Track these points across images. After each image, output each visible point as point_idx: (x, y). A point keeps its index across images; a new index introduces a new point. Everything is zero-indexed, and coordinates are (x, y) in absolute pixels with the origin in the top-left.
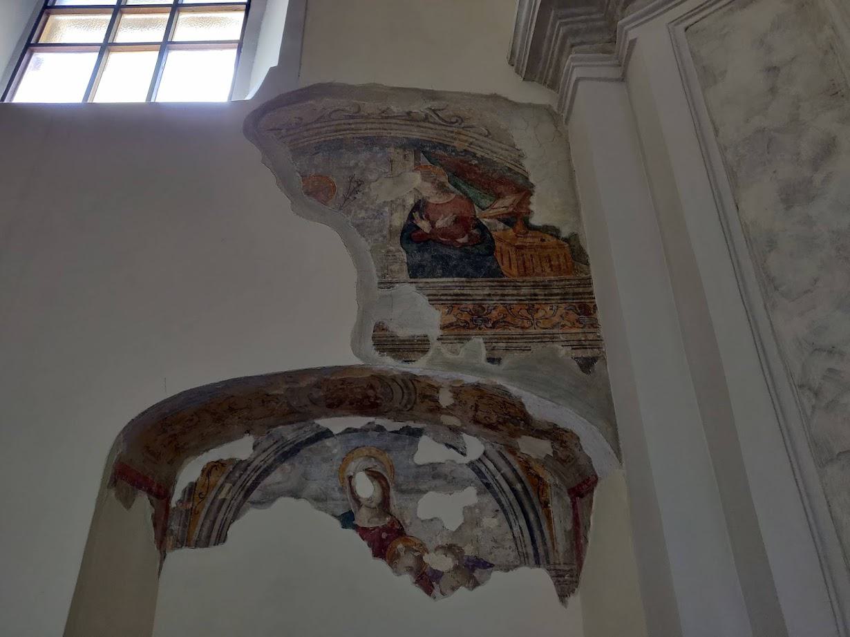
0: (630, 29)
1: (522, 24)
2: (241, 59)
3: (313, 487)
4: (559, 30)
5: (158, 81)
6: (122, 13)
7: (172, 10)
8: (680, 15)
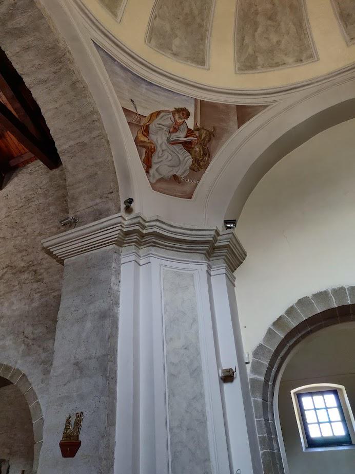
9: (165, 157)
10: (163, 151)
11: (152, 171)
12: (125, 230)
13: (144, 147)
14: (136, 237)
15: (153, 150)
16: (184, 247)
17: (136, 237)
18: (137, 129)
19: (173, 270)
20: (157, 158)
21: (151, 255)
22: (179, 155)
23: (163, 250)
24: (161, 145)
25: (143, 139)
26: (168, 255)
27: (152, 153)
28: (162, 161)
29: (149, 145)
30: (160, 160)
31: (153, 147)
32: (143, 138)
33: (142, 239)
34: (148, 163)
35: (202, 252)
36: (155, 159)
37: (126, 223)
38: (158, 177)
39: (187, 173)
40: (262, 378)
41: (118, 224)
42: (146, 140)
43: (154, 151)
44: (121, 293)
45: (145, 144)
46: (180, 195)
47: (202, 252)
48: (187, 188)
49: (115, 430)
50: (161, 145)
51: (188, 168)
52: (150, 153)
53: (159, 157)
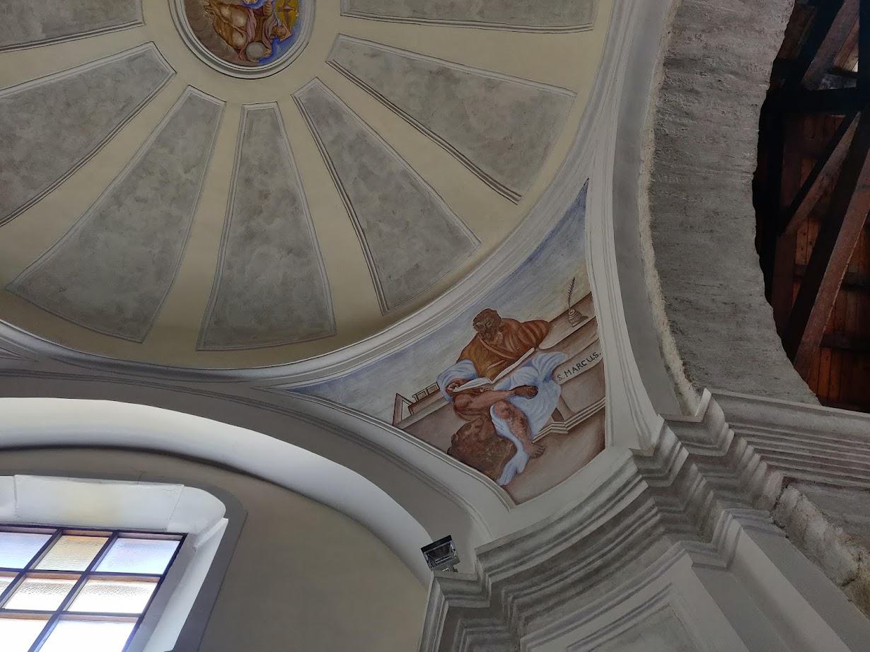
0: (533, 647)
1: (429, 633)
2: (138, 631)
3: (727, 143)
4: (465, 639)
5: (73, 597)
6: (26, 577)
7: (52, 617)
8: (577, 640)
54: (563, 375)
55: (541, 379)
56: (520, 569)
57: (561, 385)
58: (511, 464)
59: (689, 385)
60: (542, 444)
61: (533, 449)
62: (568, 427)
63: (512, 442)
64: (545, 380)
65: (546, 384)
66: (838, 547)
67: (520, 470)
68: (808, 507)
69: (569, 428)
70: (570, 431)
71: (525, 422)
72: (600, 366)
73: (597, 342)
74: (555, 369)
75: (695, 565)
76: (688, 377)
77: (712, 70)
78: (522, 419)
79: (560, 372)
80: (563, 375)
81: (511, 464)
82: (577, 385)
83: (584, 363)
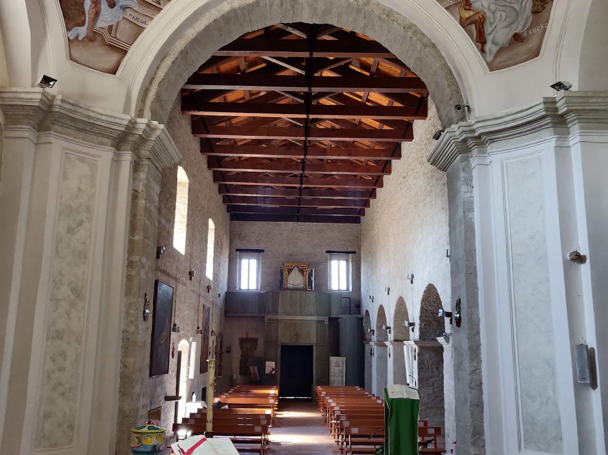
9: (498, 18)
10: (493, 13)
11: (488, 47)
12: (460, 140)
13: (471, 23)
14: (471, 142)
15: (482, 20)
16: (525, 130)
17: (471, 142)
18: (457, 9)
19: (517, 159)
20: (489, 26)
21: (491, 154)
22: (512, 5)
23: (505, 141)
24: (489, 9)
25: (467, 16)
26: (504, 147)
27: (482, 23)
28: (496, 26)
29: (476, 17)
30: (494, 26)
31: (481, 17)
32: (467, 14)
33: (481, 140)
34: (481, 40)
35: (548, 126)
36: (488, 29)
37: (457, 133)
38: (495, 49)
39: (531, 19)
40: (335, 385)
41: (449, 139)
42: (471, 13)
43: (484, 20)
44: (475, 198)
45: (472, 19)
46: (525, 57)
47: (548, 126)
48: (532, 44)
49: (478, 310)
50: (489, 9)
51: (530, 14)
52: (480, 25)
53: (491, 24)
54: (128, 14)
55: (120, 4)
56: (69, 114)
57: (124, 17)
58: (77, 30)
59: (156, 87)
60: (96, 36)
61: (91, 34)
62: (111, 42)
63: (85, 17)
64: (121, 7)
65: (119, 9)
66: (142, 183)
67: (80, 38)
68: (146, 169)
69: (110, 43)
70: (109, 45)
71: (97, 14)
72: (142, 29)
73: (152, 19)
74: (129, 7)
75: (112, 159)
76: (159, 84)
77: (293, 7)
78: (97, 11)
79: (129, 11)
80: (128, 14)
81: (77, 30)
82: (128, 25)
83: (139, 20)
